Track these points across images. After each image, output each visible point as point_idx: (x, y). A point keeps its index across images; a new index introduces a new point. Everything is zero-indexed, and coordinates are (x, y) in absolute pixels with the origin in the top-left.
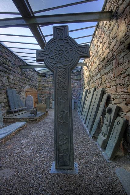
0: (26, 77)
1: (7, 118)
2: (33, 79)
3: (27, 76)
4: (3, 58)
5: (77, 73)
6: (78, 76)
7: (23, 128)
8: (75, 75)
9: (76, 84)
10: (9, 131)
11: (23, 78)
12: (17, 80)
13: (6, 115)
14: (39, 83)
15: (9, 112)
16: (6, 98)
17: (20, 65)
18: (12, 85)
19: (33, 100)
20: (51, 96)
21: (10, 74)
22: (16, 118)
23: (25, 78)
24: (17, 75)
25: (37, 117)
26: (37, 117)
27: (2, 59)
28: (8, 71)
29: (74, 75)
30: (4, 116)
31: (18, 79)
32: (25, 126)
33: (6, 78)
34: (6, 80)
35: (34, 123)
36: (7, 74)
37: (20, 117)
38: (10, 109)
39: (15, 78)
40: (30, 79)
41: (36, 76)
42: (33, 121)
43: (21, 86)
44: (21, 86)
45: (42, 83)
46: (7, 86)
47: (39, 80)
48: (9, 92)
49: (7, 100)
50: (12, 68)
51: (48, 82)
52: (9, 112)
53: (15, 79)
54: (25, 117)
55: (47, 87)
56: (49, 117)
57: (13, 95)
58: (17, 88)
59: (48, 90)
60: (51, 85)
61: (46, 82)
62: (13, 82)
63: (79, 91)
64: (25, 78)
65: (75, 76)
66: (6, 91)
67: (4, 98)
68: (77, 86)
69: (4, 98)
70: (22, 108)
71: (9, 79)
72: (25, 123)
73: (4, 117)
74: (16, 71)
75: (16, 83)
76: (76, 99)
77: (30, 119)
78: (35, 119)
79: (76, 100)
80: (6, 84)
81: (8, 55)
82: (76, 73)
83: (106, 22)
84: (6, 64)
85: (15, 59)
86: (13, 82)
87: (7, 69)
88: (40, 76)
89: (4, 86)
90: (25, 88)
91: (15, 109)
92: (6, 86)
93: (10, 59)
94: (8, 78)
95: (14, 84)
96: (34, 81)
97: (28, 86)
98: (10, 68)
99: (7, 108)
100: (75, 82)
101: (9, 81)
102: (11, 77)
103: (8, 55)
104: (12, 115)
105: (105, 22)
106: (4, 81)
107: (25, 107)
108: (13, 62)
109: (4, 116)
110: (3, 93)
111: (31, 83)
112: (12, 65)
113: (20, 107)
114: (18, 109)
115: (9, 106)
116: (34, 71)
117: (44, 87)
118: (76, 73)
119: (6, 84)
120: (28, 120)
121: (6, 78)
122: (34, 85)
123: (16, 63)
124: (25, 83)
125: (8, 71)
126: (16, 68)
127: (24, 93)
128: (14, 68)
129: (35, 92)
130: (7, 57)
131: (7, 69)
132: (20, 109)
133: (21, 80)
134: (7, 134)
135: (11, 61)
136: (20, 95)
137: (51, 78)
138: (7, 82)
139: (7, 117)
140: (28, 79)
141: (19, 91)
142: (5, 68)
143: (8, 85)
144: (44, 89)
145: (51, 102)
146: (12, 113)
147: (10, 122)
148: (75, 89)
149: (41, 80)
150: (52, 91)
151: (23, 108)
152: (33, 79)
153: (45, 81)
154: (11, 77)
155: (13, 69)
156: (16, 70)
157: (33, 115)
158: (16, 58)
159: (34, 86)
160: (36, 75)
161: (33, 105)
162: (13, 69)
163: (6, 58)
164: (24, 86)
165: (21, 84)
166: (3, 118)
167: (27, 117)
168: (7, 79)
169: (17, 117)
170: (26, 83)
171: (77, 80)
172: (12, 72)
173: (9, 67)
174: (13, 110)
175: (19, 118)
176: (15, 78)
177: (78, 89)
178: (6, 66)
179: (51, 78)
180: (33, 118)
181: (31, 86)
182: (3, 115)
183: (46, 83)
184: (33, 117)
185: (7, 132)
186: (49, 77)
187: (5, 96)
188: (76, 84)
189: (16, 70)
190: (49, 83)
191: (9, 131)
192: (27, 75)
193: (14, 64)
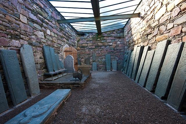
0: (65, 35)
1: (45, 84)
2: (72, 38)
3: (65, 33)
4: (38, 7)
5: (120, 30)
6: (121, 34)
7: (67, 99)
8: (118, 32)
9: (118, 43)
10: (49, 109)
11: (61, 35)
12: (54, 37)
13: (42, 79)
14: (78, 42)
15: (47, 76)
16: (42, 58)
17: (58, 19)
18: (49, 43)
19: (73, 61)
20: (91, 56)
21: (47, 28)
22: (56, 84)
23: (63, 36)
24: (55, 30)
25: (82, 81)
26: (82, 81)
27: (36, 8)
28: (44, 24)
29: (116, 33)
30: (41, 81)
31: (56, 36)
32: (70, 95)
33: (42, 33)
34: (43, 35)
35: (79, 90)
36: (43, 28)
37: (61, 82)
38: (48, 71)
39: (53, 34)
40: (69, 38)
41: (74, 35)
42: (77, 86)
43: (59, 44)
44: (59, 44)
45: (81, 42)
46: (44, 43)
47: (78, 40)
48: (46, 50)
49: (43, 61)
50: (49, 21)
51: (87, 41)
52: (47, 76)
53: (52, 35)
54: (67, 82)
55: (86, 46)
56: (93, 80)
57: (51, 55)
58: (55, 46)
59: (87, 50)
60: (91, 44)
61: (86, 42)
62: (50, 39)
63: (122, 50)
64: (63, 36)
65: (118, 33)
66: (42, 49)
67: (40, 58)
68: (120, 45)
69: (40, 58)
70: (61, 70)
71: (46, 34)
72: (69, 92)
73: (40, 82)
74: (53, 25)
75: (54, 41)
76: (119, 59)
77: (74, 84)
78: (81, 84)
79: (119, 60)
80: (42, 40)
81: (44, 4)
82: (119, 30)
83: (96, 29)
84: (41, 15)
85: (52, 11)
86: (50, 39)
87: (43, 21)
88: (78, 34)
89: (40, 43)
90: (64, 47)
91: (54, 71)
92: (43, 43)
93: (46, 10)
94: (45, 32)
95: (52, 41)
96: (73, 40)
97: (67, 45)
98: (47, 21)
99: (44, 70)
100: (118, 40)
101: (45, 37)
102: (48, 32)
103: (44, 5)
104: (50, 79)
105: (96, 28)
106: (40, 36)
107: (64, 69)
108: (50, 14)
109: (41, 81)
110: (38, 51)
111: (70, 42)
112: (48, 18)
113: (59, 70)
114: (57, 71)
115: (46, 67)
116: (72, 28)
117: (83, 47)
118: (119, 30)
119: (42, 40)
120: (71, 86)
121: (42, 33)
122: (73, 44)
123: (54, 16)
124: (64, 41)
125: (44, 24)
126: (54, 22)
127: (63, 52)
128: (51, 22)
129: (74, 52)
130: (43, 6)
131: (43, 21)
132: (59, 71)
133: (59, 38)
134: (45, 116)
135: (47, 11)
136: (59, 55)
137: (91, 36)
138: (44, 38)
139: (44, 82)
140: (67, 37)
141: (58, 50)
142: (40, 19)
143: (45, 41)
144: (83, 49)
145: (91, 63)
146: (50, 76)
147: (48, 89)
148: (118, 48)
149: (79, 39)
150: (92, 51)
151: (63, 70)
152: (72, 38)
153: (83, 40)
154: (48, 32)
155: (50, 23)
156: (54, 24)
157: (77, 78)
158: (53, 10)
159: (72, 45)
160: (74, 34)
161: (74, 66)
162: (50, 23)
163: (41, 7)
164: (62, 44)
165: (59, 42)
166: (39, 84)
167: (68, 81)
168: (43, 34)
169: (58, 82)
170: (64, 41)
171: (119, 38)
172: (49, 26)
173: (46, 20)
174: (52, 73)
175: (60, 84)
176: (53, 34)
177: (121, 48)
178: (42, 17)
179: (91, 36)
180: (78, 84)
181: (69, 45)
182: (39, 79)
183: (85, 43)
184: (77, 82)
185: (45, 112)
186: (89, 36)
187: (41, 55)
188: (118, 43)
189: (54, 24)
190: (89, 42)
191: (49, 109)
192: (66, 33)
193: (52, 17)
